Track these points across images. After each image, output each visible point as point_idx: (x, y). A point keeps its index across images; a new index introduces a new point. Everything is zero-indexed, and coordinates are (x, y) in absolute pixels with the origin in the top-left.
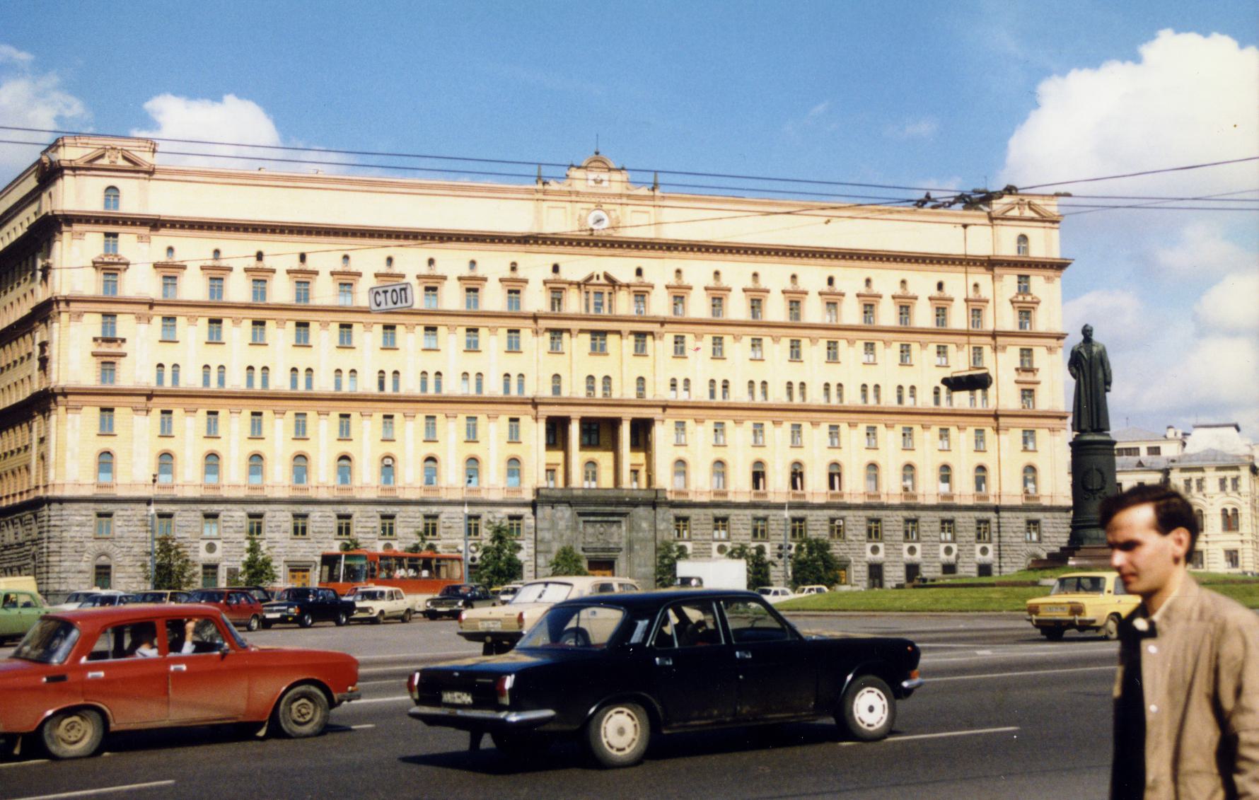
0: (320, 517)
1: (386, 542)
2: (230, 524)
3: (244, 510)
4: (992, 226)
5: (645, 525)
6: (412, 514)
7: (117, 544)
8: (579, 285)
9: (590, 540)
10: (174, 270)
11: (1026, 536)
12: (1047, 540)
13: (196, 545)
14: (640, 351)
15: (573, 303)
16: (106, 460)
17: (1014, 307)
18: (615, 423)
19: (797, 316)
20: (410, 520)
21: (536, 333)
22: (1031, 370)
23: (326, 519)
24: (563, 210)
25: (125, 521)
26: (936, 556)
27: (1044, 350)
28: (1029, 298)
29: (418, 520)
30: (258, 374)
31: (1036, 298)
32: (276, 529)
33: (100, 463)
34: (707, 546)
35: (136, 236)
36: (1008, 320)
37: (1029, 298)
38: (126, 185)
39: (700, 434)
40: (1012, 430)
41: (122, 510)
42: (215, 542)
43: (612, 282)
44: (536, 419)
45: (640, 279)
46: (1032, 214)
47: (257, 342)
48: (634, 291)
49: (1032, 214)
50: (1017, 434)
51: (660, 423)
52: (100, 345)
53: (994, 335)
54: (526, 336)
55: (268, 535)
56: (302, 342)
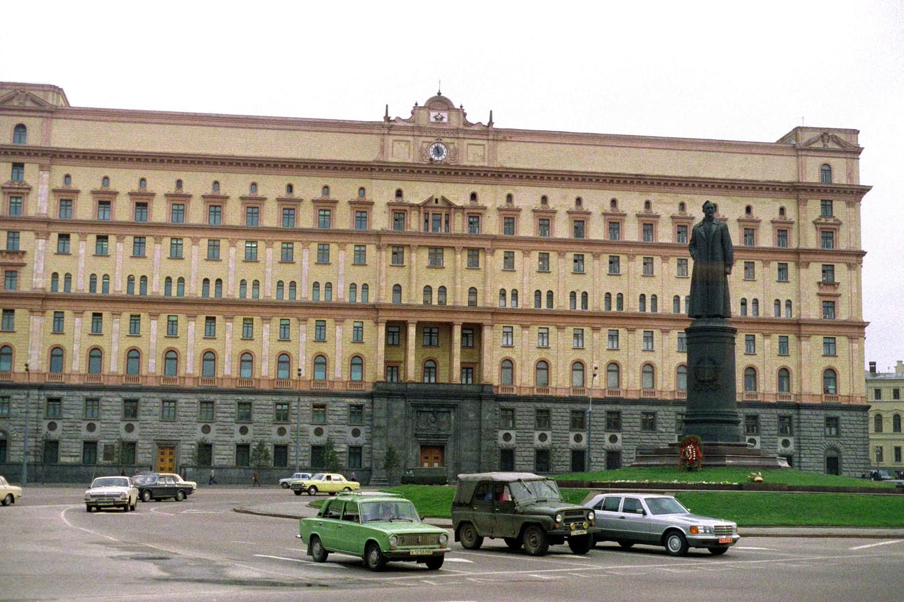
0: (186, 403)
1: (128, 422)
2: (109, 408)
3: (120, 396)
4: (798, 156)
5: (472, 415)
6: (264, 402)
7: (12, 422)
8: (418, 206)
9: (423, 427)
10: (181, 199)
11: (825, 432)
12: (844, 435)
13: (79, 425)
14: (473, 265)
15: (414, 223)
16: (830, 375)
17: (817, 228)
18: (449, 326)
19: (752, 242)
20: (263, 407)
21: (379, 248)
22: (834, 285)
23: (191, 405)
24: (482, 147)
25: (19, 403)
26: (567, 442)
27: (844, 266)
28: (831, 221)
29: (270, 407)
30: (750, 306)
31: (837, 220)
32: (147, 413)
33: (746, 375)
34: (601, 436)
35: (37, 165)
36: (812, 240)
37: (831, 221)
38: (33, 124)
39: (768, 345)
40: (813, 338)
41: (18, 394)
42: (95, 423)
43: (449, 205)
44: (377, 323)
45: (474, 203)
46: (837, 147)
47: (63, 252)
48: (468, 213)
49: (837, 147)
50: (819, 340)
51: (490, 327)
52: (822, 288)
53: (798, 252)
54: (371, 250)
55: (142, 418)
56: (436, 263)
